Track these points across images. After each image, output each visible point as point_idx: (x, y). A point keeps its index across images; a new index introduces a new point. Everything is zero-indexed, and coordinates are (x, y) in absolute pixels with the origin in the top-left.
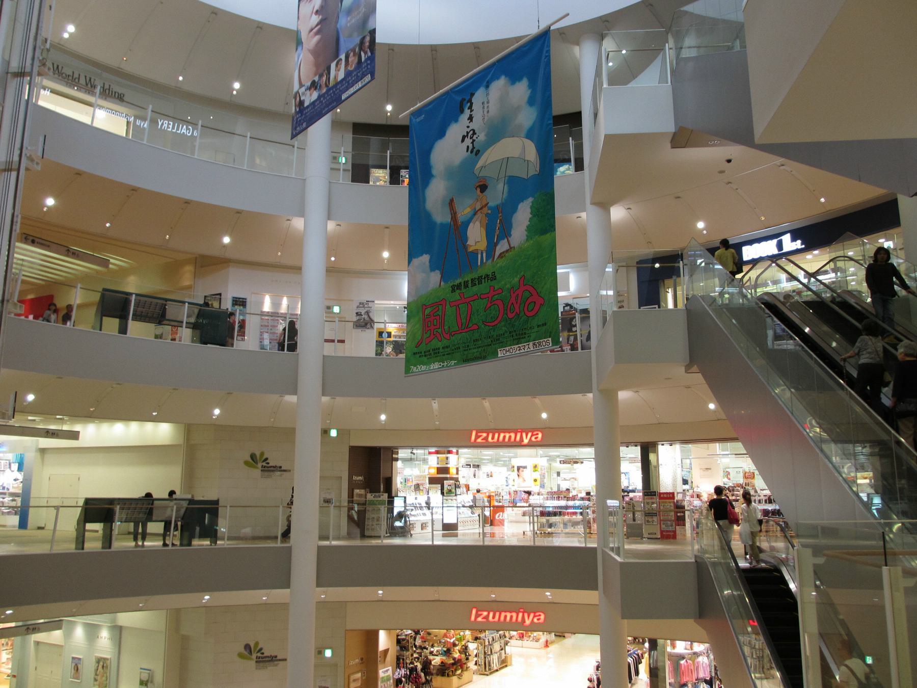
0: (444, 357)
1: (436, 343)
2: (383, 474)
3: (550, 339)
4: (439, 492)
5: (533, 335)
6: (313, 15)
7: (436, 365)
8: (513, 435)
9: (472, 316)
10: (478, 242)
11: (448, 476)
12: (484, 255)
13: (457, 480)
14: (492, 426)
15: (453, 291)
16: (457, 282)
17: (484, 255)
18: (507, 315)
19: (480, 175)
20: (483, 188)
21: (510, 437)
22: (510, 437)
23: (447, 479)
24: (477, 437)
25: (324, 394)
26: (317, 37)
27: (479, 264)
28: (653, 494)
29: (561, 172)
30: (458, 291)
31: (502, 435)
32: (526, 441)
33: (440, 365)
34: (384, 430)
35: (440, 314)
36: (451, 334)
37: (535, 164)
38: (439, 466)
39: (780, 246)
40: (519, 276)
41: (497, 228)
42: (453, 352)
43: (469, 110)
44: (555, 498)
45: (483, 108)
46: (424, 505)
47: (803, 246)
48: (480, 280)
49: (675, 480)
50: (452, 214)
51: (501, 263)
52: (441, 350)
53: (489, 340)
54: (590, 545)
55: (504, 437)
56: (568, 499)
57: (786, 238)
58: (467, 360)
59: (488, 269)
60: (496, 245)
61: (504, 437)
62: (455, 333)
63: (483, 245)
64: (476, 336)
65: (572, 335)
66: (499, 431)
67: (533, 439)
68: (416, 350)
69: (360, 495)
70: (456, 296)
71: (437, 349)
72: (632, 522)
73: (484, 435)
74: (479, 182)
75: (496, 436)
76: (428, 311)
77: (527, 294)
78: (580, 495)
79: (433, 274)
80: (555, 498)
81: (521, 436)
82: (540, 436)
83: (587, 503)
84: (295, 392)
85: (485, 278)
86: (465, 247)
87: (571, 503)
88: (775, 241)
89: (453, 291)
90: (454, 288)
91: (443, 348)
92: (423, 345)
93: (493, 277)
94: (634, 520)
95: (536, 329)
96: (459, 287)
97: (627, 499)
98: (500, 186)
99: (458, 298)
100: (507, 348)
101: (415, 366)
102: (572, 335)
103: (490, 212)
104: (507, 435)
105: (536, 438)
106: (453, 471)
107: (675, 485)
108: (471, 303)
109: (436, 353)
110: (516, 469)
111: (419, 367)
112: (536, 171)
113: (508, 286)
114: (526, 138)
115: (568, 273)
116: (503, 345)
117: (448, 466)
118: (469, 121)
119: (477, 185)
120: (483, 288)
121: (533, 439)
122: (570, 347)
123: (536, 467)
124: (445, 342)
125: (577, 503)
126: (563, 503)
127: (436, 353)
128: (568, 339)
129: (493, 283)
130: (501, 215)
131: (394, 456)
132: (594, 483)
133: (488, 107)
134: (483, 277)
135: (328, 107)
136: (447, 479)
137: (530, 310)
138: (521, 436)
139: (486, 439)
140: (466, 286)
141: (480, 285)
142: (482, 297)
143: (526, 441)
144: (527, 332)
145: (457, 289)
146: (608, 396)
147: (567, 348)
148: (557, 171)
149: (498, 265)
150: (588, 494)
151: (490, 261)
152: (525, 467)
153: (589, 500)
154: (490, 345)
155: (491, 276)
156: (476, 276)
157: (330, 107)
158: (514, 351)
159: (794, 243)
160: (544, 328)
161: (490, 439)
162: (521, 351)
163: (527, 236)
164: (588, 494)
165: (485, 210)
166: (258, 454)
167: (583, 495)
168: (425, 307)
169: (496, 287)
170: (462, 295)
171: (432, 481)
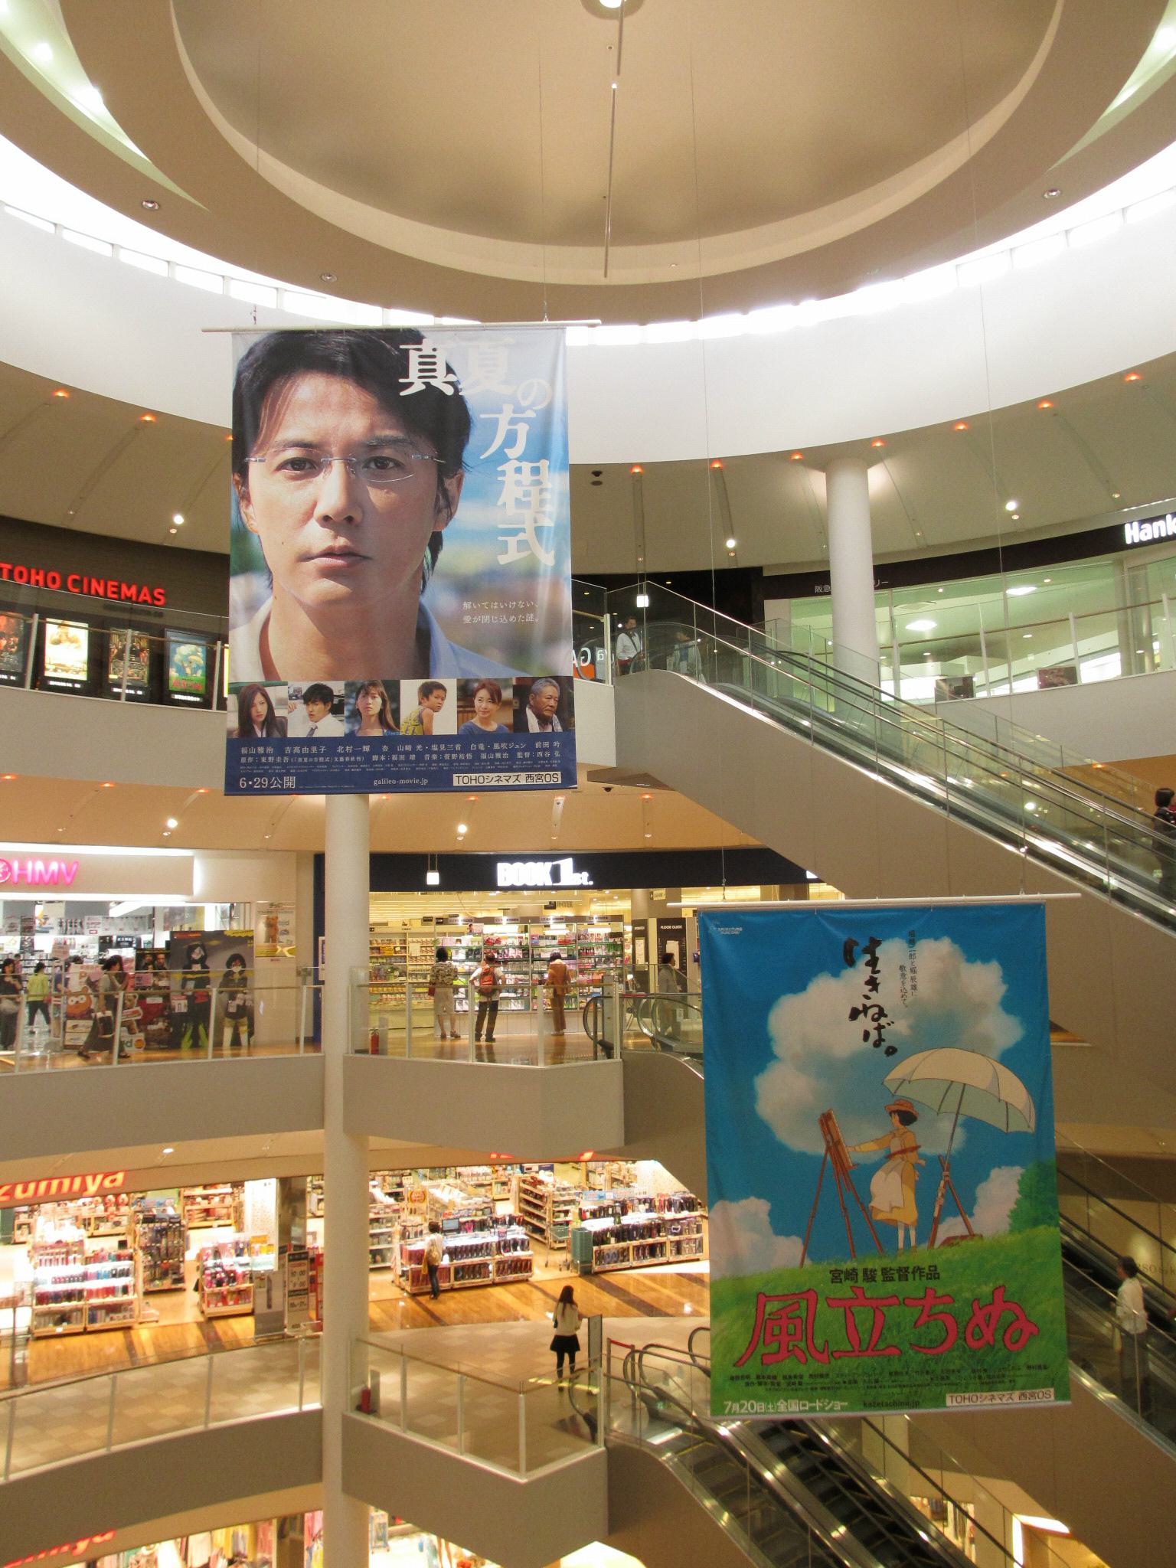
0: (814, 1393)
1: (789, 1366)
3: (1052, 1390)
5: (1020, 1381)
9: (884, 1331)
10: (898, 1208)
12: (913, 1233)
16: (849, 1265)
17: (913, 1233)
18: (965, 1340)
19: (899, 1093)
20: (907, 1118)
26: (328, 586)
27: (901, 1245)
28: (303, 1256)
29: (182, 655)
30: (849, 1283)
33: (804, 1405)
35: (804, 1315)
36: (827, 1353)
37: (1027, 1117)
39: (555, 874)
40: (991, 1285)
41: (940, 1195)
42: (837, 1385)
43: (870, 969)
44: (60, 1261)
45: (903, 975)
47: (591, 883)
48: (903, 1273)
50: (828, 1142)
52: (806, 1379)
53: (928, 1377)
54: (307, 1407)
57: (566, 865)
59: (922, 1256)
60: (936, 1222)
62: (838, 1354)
63: (909, 1214)
64: (897, 1366)
65: (191, 979)
68: (735, 1371)
70: (845, 1290)
71: (795, 1377)
72: (266, 1310)
74: (895, 1104)
75: (32, 1186)
76: (771, 1307)
77: (1008, 1316)
80: (60, 1261)
83: (125, 1264)
85: (914, 1272)
86: (866, 1211)
87: (93, 1268)
88: (549, 865)
90: (836, 1276)
91: (811, 1376)
93: (933, 1273)
94: (269, 1306)
95: (1024, 1371)
96: (851, 1274)
98: (946, 1126)
99: (850, 1294)
100: (967, 1395)
101: (735, 1400)
102: (191, 979)
103: (923, 1162)
105: (113, 1181)
108: (884, 1309)
109: (794, 1384)
111: (748, 1405)
112: (1029, 1127)
113: (967, 1295)
114: (1001, 1063)
115: (191, 860)
118: (870, 987)
119: (896, 1108)
120: (913, 1287)
122: (186, 1001)
124: (814, 1366)
127: (794, 1384)
128: (183, 986)
129: (932, 1284)
130: (947, 1173)
133: (913, 979)
134: (910, 1270)
135: (398, 780)
137: (1013, 1341)
141: (903, 1283)
142: (907, 1302)
144: (1007, 1373)
145: (847, 1278)
147: (180, 1004)
148: (175, 653)
149: (943, 1257)
151: (925, 1246)
154: (929, 1385)
155: (927, 1271)
156: (895, 1265)
157: (401, 782)
158: (979, 1400)
159: (578, 875)
160: (1044, 1372)
162: (994, 1402)
163: (1010, 1225)
165: (912, 1157)
168: (762, 1298)
169: (940, 1293)
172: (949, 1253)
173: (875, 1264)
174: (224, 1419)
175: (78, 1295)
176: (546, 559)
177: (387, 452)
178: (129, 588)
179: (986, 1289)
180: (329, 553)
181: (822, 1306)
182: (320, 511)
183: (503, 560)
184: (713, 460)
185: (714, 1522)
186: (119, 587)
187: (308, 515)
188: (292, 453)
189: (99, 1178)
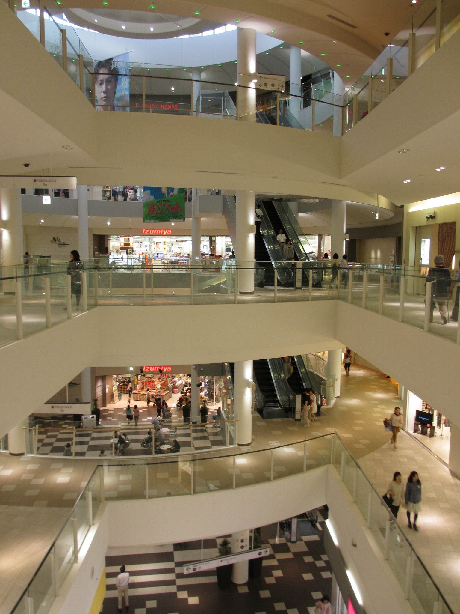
1: (152, 215)
2: (106, 246)
4: (126, 253)
6: (102, 93)
7: (153, 221)
8: (160, 231)
11: (129, 246)
13: (132, 248)
14: (152, 228)
15: (157, 202)
21: (159, 232)
22: (159, 232)
23: (129, 248)
24: (145, 231)
25: (89, 216)
31: (155, 231)
32: (165, 234)
34: (108, 228)
38: (125, 242)
46: (120, 258)
48: (165, 201)
49: (222, 250)
51: (171, 198)
55: (156, 232)
56: (180, 257)
58: (161, 221)
59: (167, 198)
60: (170, 193)
61: (156, 232)
66: (154, 229)
67: (168, 233)
68: (146, 216)
69: (97, 254)
70: (158, 204)
73: (148, 231)
76: (150, 206)
78: (185, 255)
79: (151, 196)
81: (163, 232)
82: (170, 232)
83: (188, 258)
84: (77, 215)
87: (181, 258)
89: (157, 202)
90: (158, 202)
92: (149, 215)
96: (159, 201)
97: (204, 257)
104: (157, 231)
106: (131, 244)
107: (222, 252)
110: (155, 243)
116: (171, 218)
117: (129, 242)
120: (166, 203)
121: (168, 233)
123: (165, 242)
124: (155, 215)
125: (184, 258)
126: (178, 258)
131: (109, 238)
132: (191, 250)
136: (129, 248)
138: (163, 232)
139: (149, 232)
140: (161, 202)
143: (165, 234)
146: (197, 220)
150: (188, 255)
152: (160, 243)
153: (189, 257)
161: (150, 232)
164: (188, 255)
166: (56, 238)
167: (186, 255)
168: (149, 205)
170: (160, 204)
171: (122, 248)
172: (171, 198)
173: (162, 200)
174: (193, 285)
175: (177, 263)
176: (127, 93)
177: (110, 79)
178: (169, 106)
179: (175, 203)
180: (104, 97)
181: (156, 206)
182: (103, 91)
183: (122, 94)
184: (265, 52)
185: (108, 220)
186: (167, 106)
187: (102, 92)
188: (100, 82)
189: (166, 231)
